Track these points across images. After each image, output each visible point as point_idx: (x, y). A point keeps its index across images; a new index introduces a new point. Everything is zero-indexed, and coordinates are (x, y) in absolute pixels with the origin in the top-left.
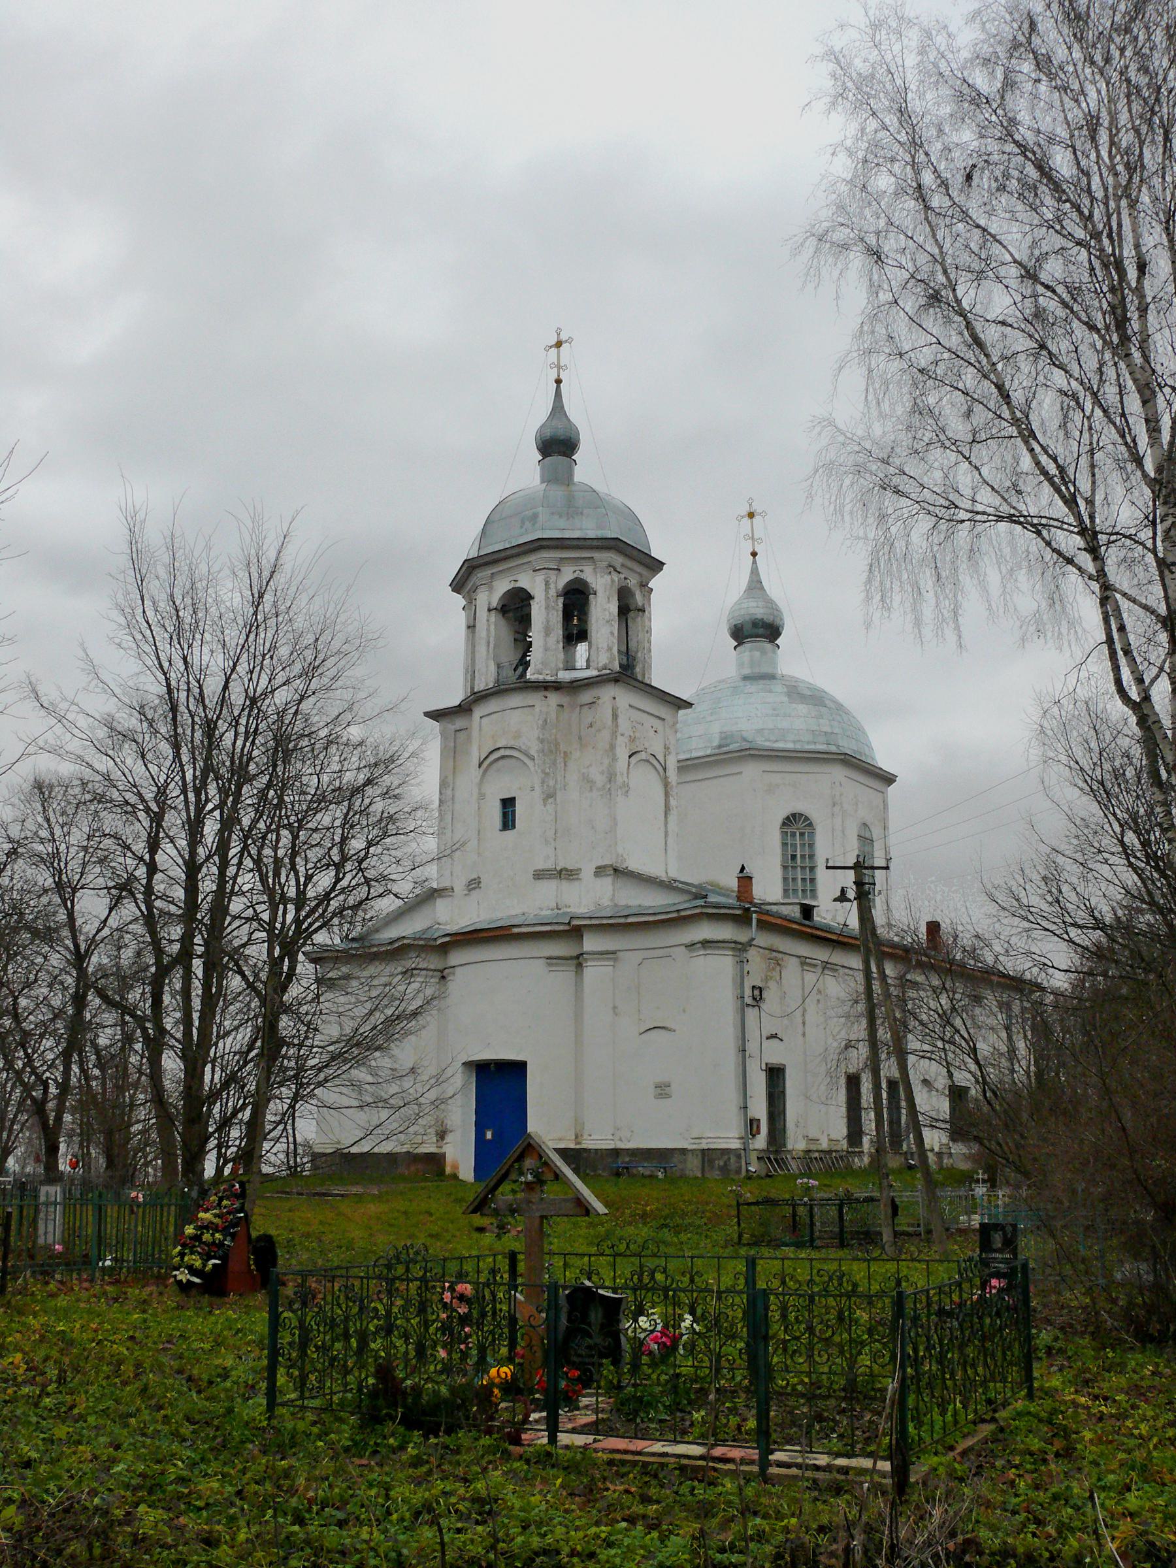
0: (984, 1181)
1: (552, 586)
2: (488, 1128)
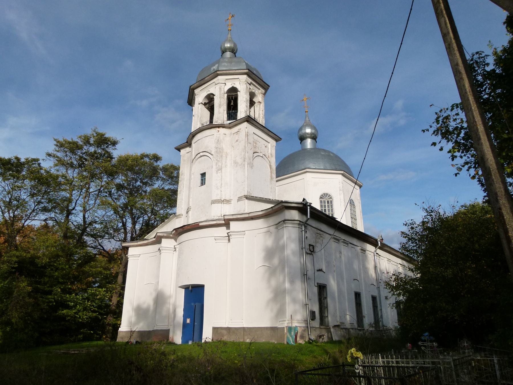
1: (222, 89)
2: (188, 318)
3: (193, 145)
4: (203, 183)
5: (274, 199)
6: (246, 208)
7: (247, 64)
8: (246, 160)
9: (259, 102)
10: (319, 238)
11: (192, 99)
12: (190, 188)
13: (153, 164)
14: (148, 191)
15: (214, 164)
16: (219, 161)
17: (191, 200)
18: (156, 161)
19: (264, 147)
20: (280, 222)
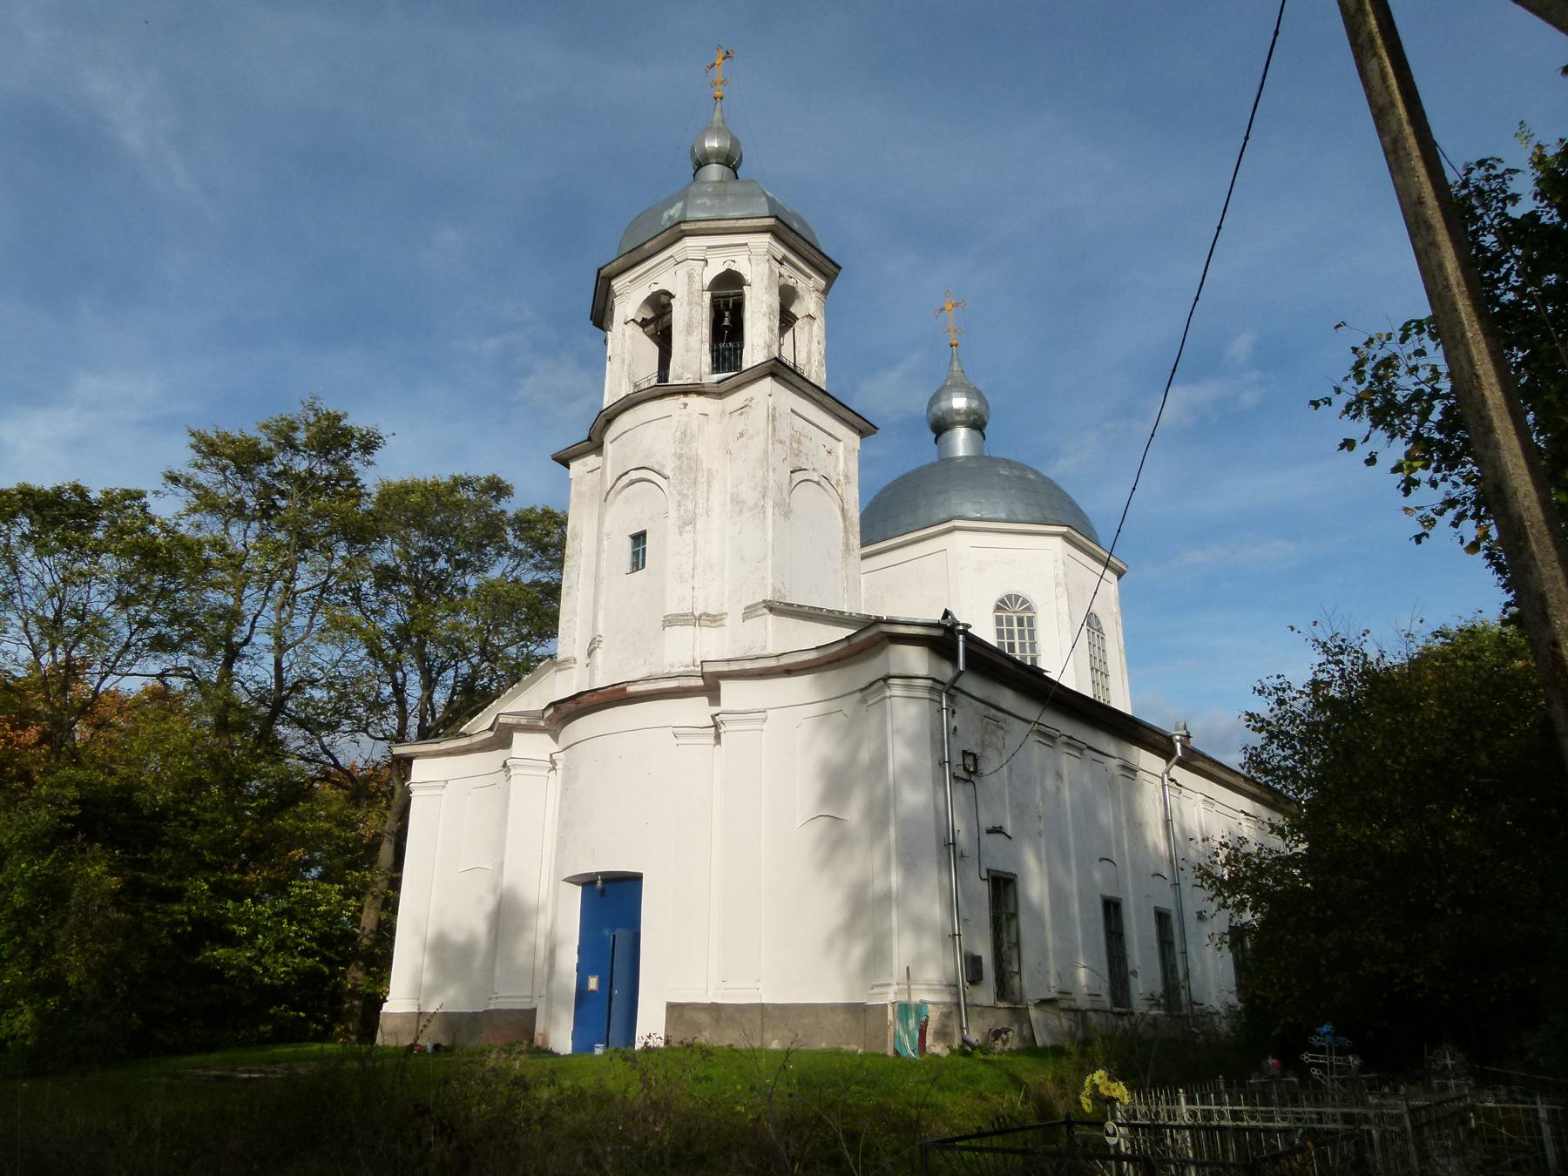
0: (54, 661)
1: (697, 279)
2: (593, 974)
3: (609, 447)
4: (638, 562)
5: (854, 612)
7: (771, 202)
8: (769, 493)
10: (993, 732)
12: (597, 580)
13: (485, 505)
15: (672, 506)
17: (601, 614)
18: (497, 499)
20: (871, 684)
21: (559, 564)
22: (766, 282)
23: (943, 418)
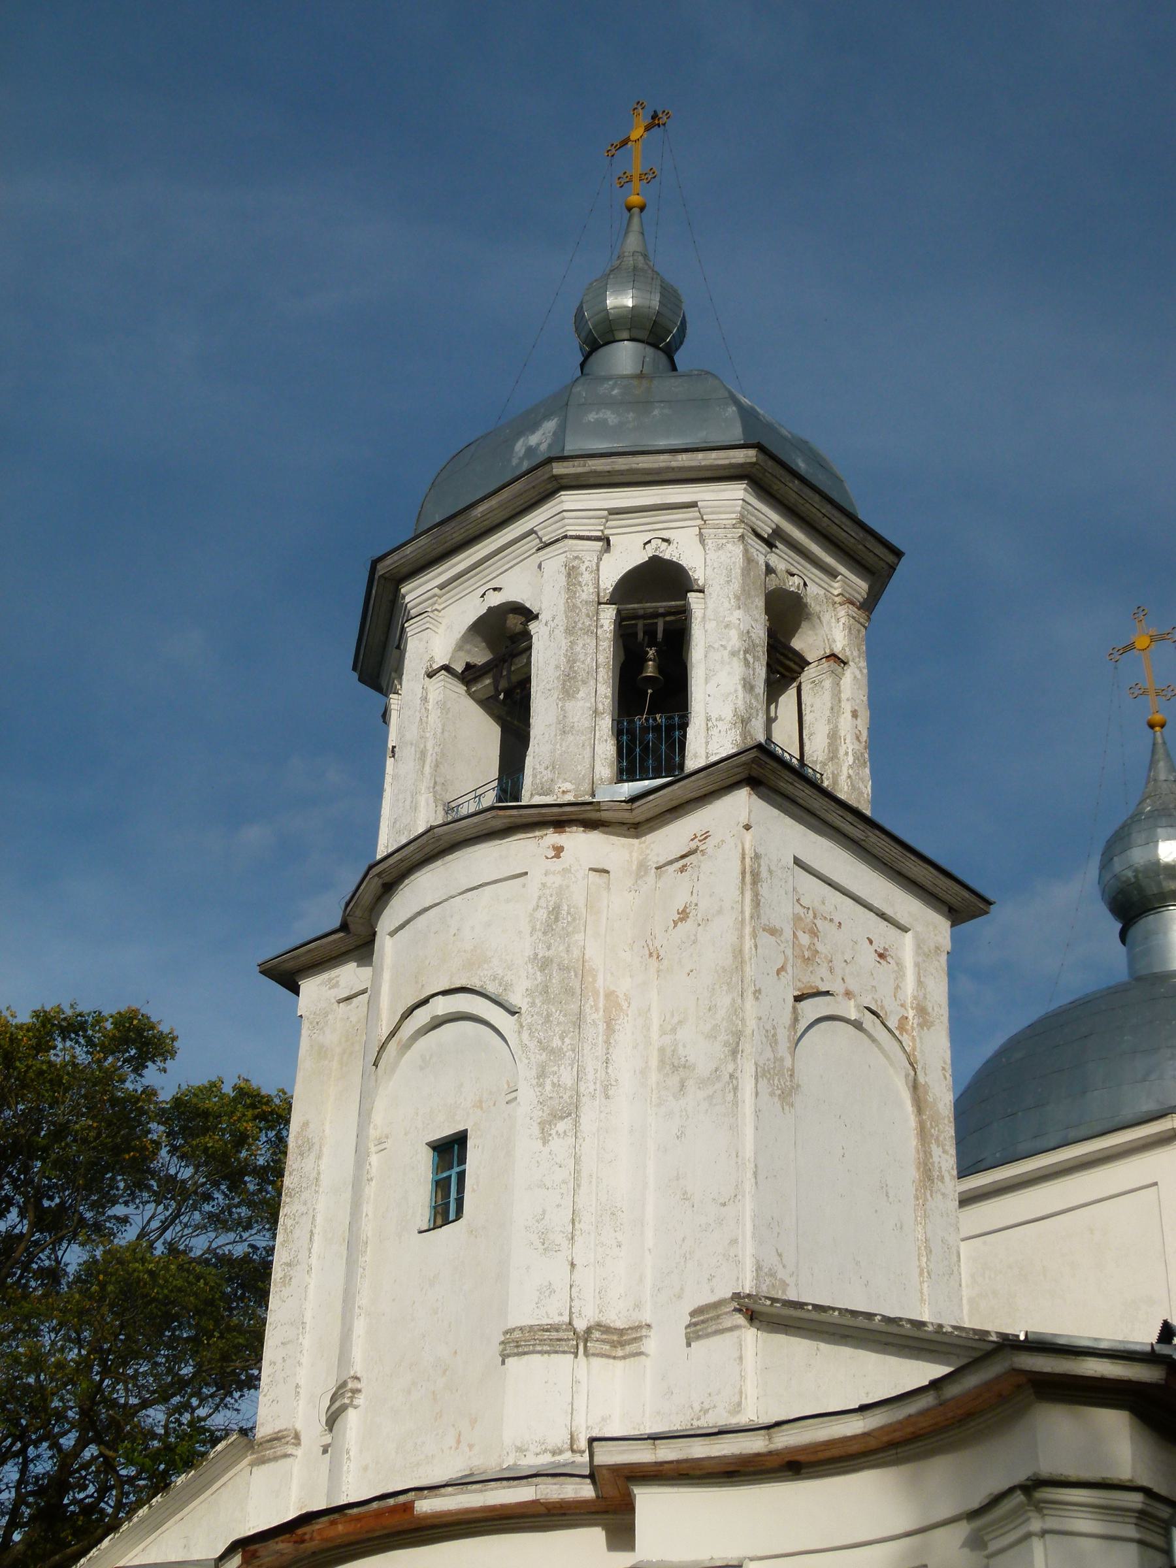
1: (587, 577)
3: (387, 946)
4: (447, 1204)
5: (948, 1321)
6: (751, 1390)
7: (748, 416)
8: (747, 1047)
9: (833, 657)
11: (385, 645)
12: (353, 1245)
13: (109, 1078)
14: (71, 1269)
15: (525, 1074)
16: (556, 1054)
17: (360, 1327)
18: (139, 1066)
19: (867, 956)
20: (996, 1500)
21: (268, 1212)
22: (736, 585)
23: (1137, 885)
